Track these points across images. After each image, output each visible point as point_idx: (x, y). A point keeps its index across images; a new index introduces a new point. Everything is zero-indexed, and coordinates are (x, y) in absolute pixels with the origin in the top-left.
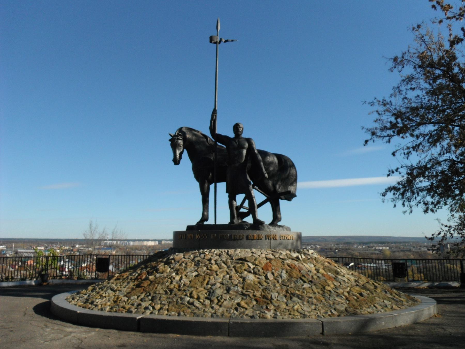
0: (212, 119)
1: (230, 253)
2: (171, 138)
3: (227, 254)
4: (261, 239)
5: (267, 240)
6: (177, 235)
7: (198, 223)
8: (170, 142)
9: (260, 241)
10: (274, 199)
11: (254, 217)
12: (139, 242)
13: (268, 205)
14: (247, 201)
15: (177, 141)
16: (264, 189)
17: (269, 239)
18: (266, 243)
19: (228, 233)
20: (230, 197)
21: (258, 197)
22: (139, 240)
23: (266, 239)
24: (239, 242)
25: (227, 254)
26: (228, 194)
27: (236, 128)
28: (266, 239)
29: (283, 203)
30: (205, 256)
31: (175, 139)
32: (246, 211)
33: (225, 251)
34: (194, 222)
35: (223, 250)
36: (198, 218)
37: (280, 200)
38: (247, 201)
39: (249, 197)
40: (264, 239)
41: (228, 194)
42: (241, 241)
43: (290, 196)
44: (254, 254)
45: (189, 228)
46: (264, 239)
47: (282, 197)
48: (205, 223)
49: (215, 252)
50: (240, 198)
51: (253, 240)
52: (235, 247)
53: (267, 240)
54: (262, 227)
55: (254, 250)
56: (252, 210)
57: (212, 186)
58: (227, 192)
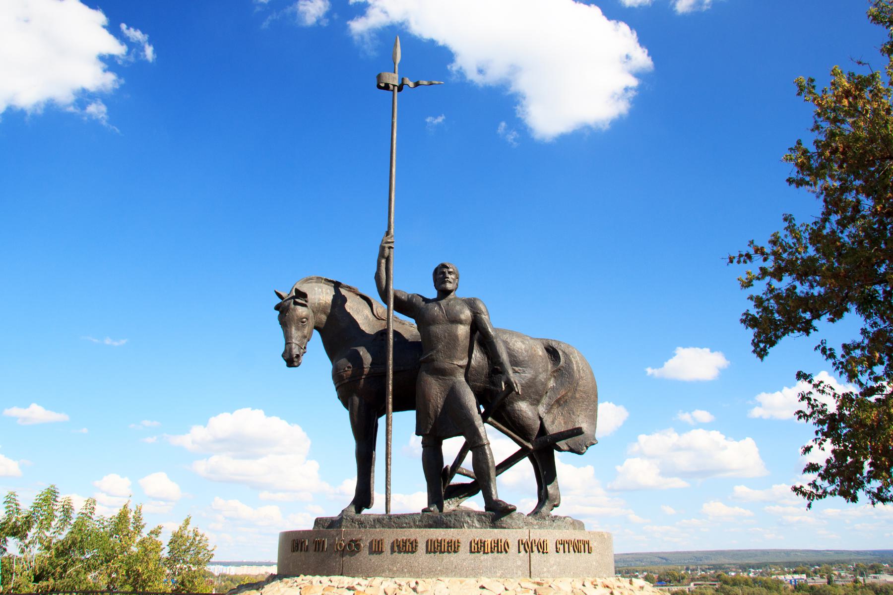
8: (278, 313)
10: (541, 451)
11: (488, 497)
12: (225, 567)
13: (525, 466)
14: (470, 455)
15: (295, 310)
16: (513, 425)
18: (519, 563)
21: (500, 445)
22: (239, 564)
23: (519, 552)
27: (440, 275)
28: (519, 552)
29: (562, 460)
32: (469, 480)
34: (334, 512)
35: (403, 581)
37: (556, 452)
38: (470, 455)
39: (475, 444)
46: (513, 549)
47: (562, 444)
48: (358, 26)
49: (382, 587)
50: (451, 447)
55: (484, 581)
56: (481, 482)
57: (382, 421)
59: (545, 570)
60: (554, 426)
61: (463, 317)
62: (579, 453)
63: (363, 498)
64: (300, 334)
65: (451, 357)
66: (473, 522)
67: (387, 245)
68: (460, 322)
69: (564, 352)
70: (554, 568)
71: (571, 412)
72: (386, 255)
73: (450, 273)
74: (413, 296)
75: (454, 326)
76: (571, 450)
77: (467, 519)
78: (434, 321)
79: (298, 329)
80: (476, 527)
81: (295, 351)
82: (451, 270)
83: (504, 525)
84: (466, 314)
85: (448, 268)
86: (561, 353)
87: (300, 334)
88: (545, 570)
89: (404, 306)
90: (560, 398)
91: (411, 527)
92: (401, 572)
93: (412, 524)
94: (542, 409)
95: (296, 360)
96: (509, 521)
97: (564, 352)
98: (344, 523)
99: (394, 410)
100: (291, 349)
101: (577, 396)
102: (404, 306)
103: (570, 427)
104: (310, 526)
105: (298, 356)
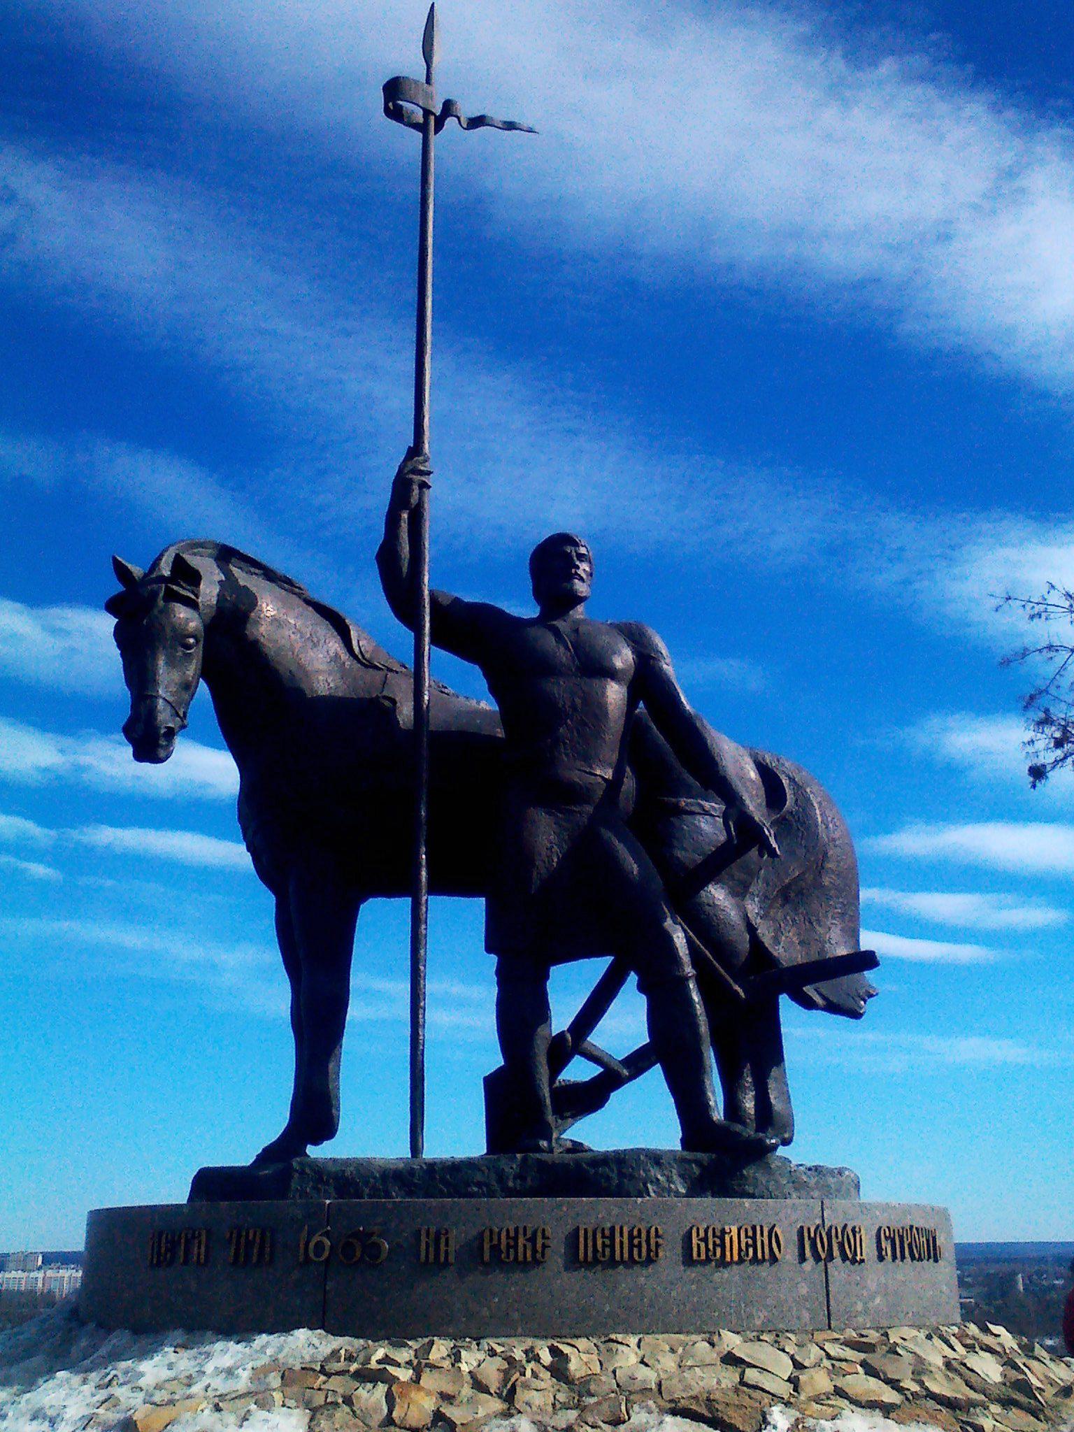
0: (289, 582)
1: (576, 1366)
2: (119, 588)
3: (559, 1370)
4: (774, 1259)
5: (809, 1264)
6: (113, 1227)
7: (267, 1155)
9: (764, 1270)
15: (166, 612)
17: (817, 1258)
18: (804, 1290)
19: (465, 1220)
20: (504, 977)
23: (802, 1259)
24: (627, 1281)
25: (559, 1370)
26: (494, 959)
28: (802, 1259)
30: (390, 1398)
31: (154, 594)
33: (532, 1355)
34: (240, 1151)
36: (272, 1121)
40: (788, 1254)
41: (494, 959)
42: (642, 1277)
43: (838, 980)
44: (752, 1375)
45: (209, 1183)
46: (788, 1254)
51: (723, 1264)
52: (603, 1327)
53: (809, 1264)
54: (762, 1179)
58: (489, 949)
59: (860, 1307)
60: (787, 950)
61: (618, 663)
62: (855, 1015)
63: (314, 1111)
64: (176, 676)
65: (587, 758)
66: (669, 1180)
67: (416, 478)
68: (612, 674)
69: (792, 780)
70: (878, 1300)
71: (811, 921)
72: (414, 499)
73: (581, 557)
74: (989, 353)
75: (596, 682)
76: (833, 1008)
77: (655, 1173)
78: (547, 668)
79: (171, 663)
80: (678, 1195)
81: (164, 717)
82: (583, 550)
83: (750, 1189)
84: (623, 658)
85: (576, 544)
86: (785, 782)
87: (176, 676)
88: (860, 1307)
89: (466, 629)
90: (788, 886)
91: (491, 1194)
92: (505, 1326)
93: (496, 1187)
94: (753, 908)
95: (163, 742)
96: (762, 1179)
97: (792, 780)
98: (294, 1185)
99: (434, 889)
100: (152, 712)
101: (826, 881)
102: (466, 629)
103: (814, 957)
104: (174, 1191)
105: (170, 734)
